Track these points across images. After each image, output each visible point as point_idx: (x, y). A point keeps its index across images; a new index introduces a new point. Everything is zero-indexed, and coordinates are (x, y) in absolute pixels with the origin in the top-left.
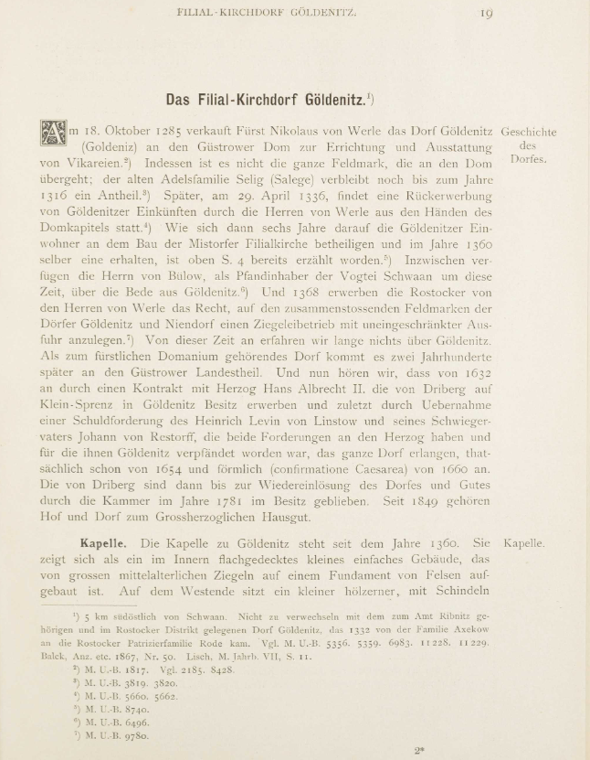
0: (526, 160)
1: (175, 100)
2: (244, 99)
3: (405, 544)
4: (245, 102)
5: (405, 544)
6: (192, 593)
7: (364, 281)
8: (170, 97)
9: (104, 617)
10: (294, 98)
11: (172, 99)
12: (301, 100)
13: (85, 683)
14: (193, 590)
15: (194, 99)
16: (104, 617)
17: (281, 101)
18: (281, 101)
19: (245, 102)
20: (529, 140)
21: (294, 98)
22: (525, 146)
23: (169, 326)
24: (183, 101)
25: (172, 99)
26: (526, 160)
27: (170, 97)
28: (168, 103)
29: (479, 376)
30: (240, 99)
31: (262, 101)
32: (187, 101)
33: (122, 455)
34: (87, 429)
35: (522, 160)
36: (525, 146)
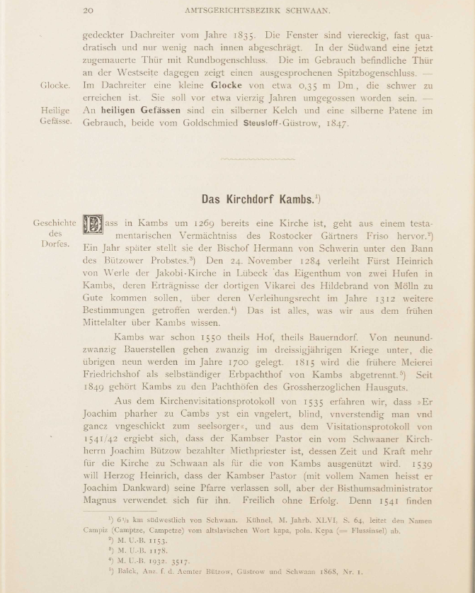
0: (53, 245)
1: (209, 200)
2: (232, 199)
3: (214, 35)
4: (233, 201)
5: (214, 35)
6: (113, 274)
7: (131, 429)
8: (205, 197)
9: (140, 521)
10: (271, 197)
11: (206, 199)
12: (276, 199)
13: (117, 540)
14: (114, 272)
15: (223, 199)
16: (140, 521)
17: (261, 200)
18: (261, 200)
19: (233, 201)
20: (57, 229)
21: (271, 197)
22: (53, 234)
23: (362, 477)
24: (214, 200)
25: (206, 199)
26: (53, 245)
27: (205, 197)
28: (203, 202)
29: (244, 37)
30: (229, 199)
31: (246, 200)
32: (218, 200)
33: (87, 124)
34: (162, 267)
35: (51, 245)
36: (53, 234)
